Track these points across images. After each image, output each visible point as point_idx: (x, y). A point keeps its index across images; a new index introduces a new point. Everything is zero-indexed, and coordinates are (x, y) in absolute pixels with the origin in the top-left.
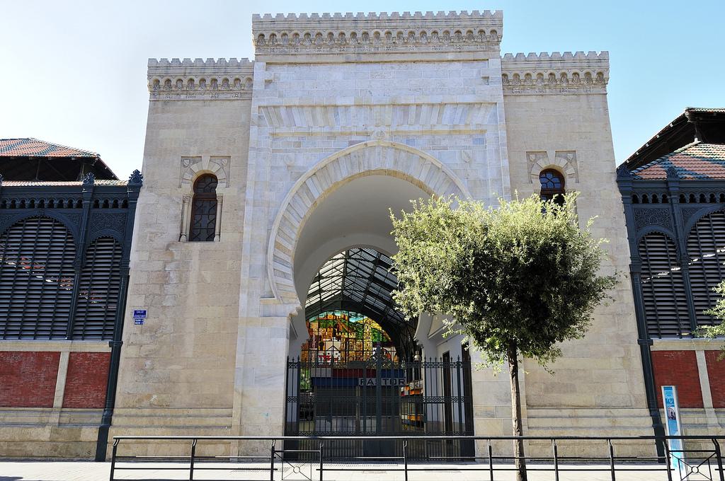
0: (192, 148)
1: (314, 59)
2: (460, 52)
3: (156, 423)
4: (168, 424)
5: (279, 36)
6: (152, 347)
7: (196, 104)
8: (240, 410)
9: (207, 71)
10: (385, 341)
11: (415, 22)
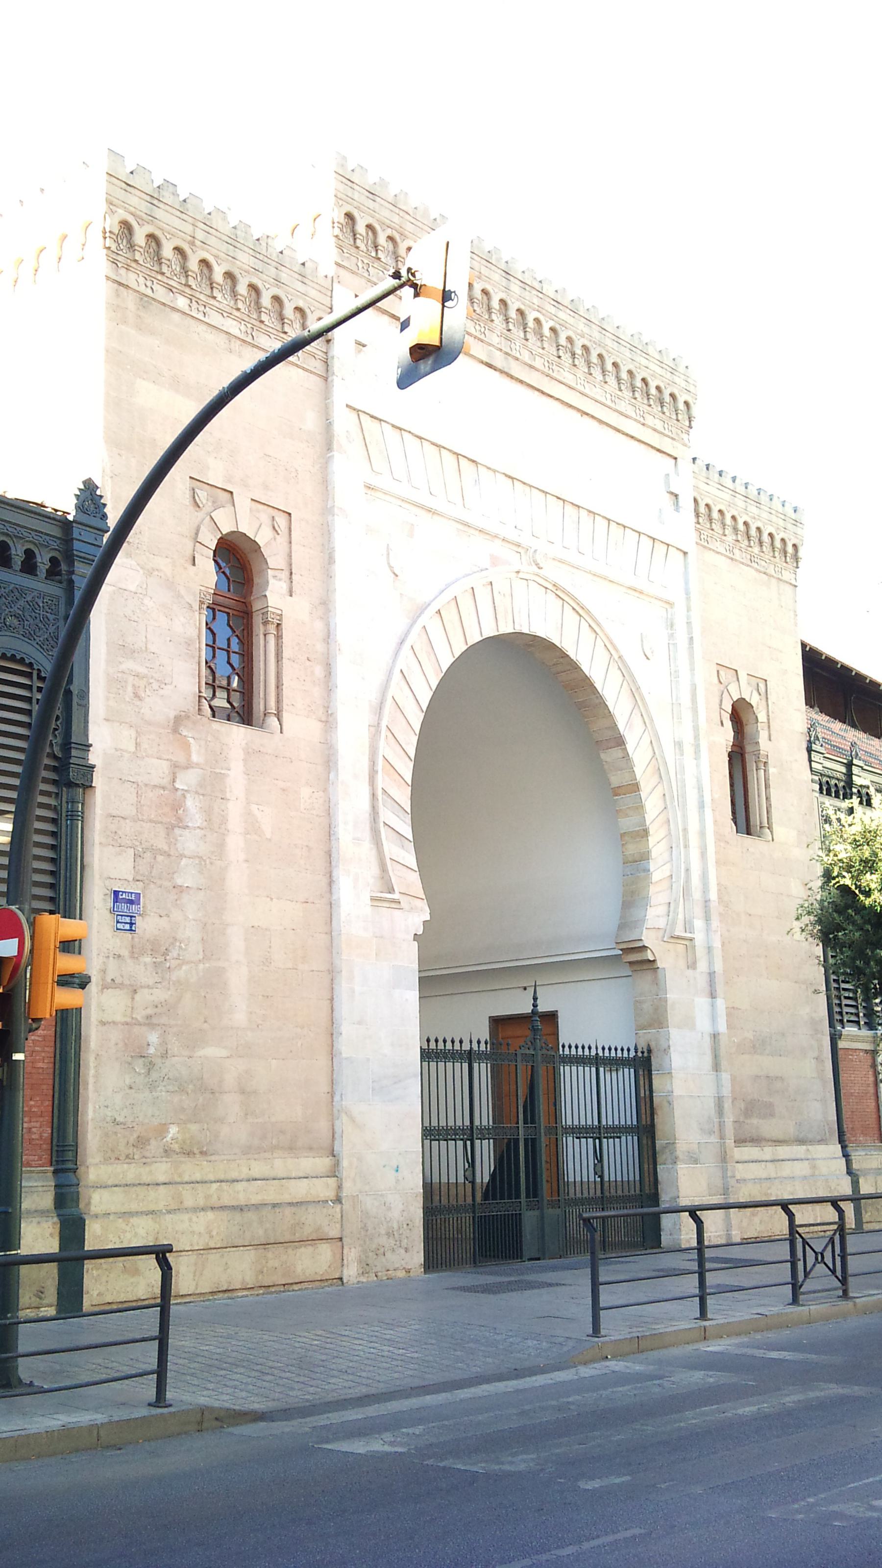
3: (189, 1202)
4: (214, 1201)
6: (160, 995)
7: (212, 337)
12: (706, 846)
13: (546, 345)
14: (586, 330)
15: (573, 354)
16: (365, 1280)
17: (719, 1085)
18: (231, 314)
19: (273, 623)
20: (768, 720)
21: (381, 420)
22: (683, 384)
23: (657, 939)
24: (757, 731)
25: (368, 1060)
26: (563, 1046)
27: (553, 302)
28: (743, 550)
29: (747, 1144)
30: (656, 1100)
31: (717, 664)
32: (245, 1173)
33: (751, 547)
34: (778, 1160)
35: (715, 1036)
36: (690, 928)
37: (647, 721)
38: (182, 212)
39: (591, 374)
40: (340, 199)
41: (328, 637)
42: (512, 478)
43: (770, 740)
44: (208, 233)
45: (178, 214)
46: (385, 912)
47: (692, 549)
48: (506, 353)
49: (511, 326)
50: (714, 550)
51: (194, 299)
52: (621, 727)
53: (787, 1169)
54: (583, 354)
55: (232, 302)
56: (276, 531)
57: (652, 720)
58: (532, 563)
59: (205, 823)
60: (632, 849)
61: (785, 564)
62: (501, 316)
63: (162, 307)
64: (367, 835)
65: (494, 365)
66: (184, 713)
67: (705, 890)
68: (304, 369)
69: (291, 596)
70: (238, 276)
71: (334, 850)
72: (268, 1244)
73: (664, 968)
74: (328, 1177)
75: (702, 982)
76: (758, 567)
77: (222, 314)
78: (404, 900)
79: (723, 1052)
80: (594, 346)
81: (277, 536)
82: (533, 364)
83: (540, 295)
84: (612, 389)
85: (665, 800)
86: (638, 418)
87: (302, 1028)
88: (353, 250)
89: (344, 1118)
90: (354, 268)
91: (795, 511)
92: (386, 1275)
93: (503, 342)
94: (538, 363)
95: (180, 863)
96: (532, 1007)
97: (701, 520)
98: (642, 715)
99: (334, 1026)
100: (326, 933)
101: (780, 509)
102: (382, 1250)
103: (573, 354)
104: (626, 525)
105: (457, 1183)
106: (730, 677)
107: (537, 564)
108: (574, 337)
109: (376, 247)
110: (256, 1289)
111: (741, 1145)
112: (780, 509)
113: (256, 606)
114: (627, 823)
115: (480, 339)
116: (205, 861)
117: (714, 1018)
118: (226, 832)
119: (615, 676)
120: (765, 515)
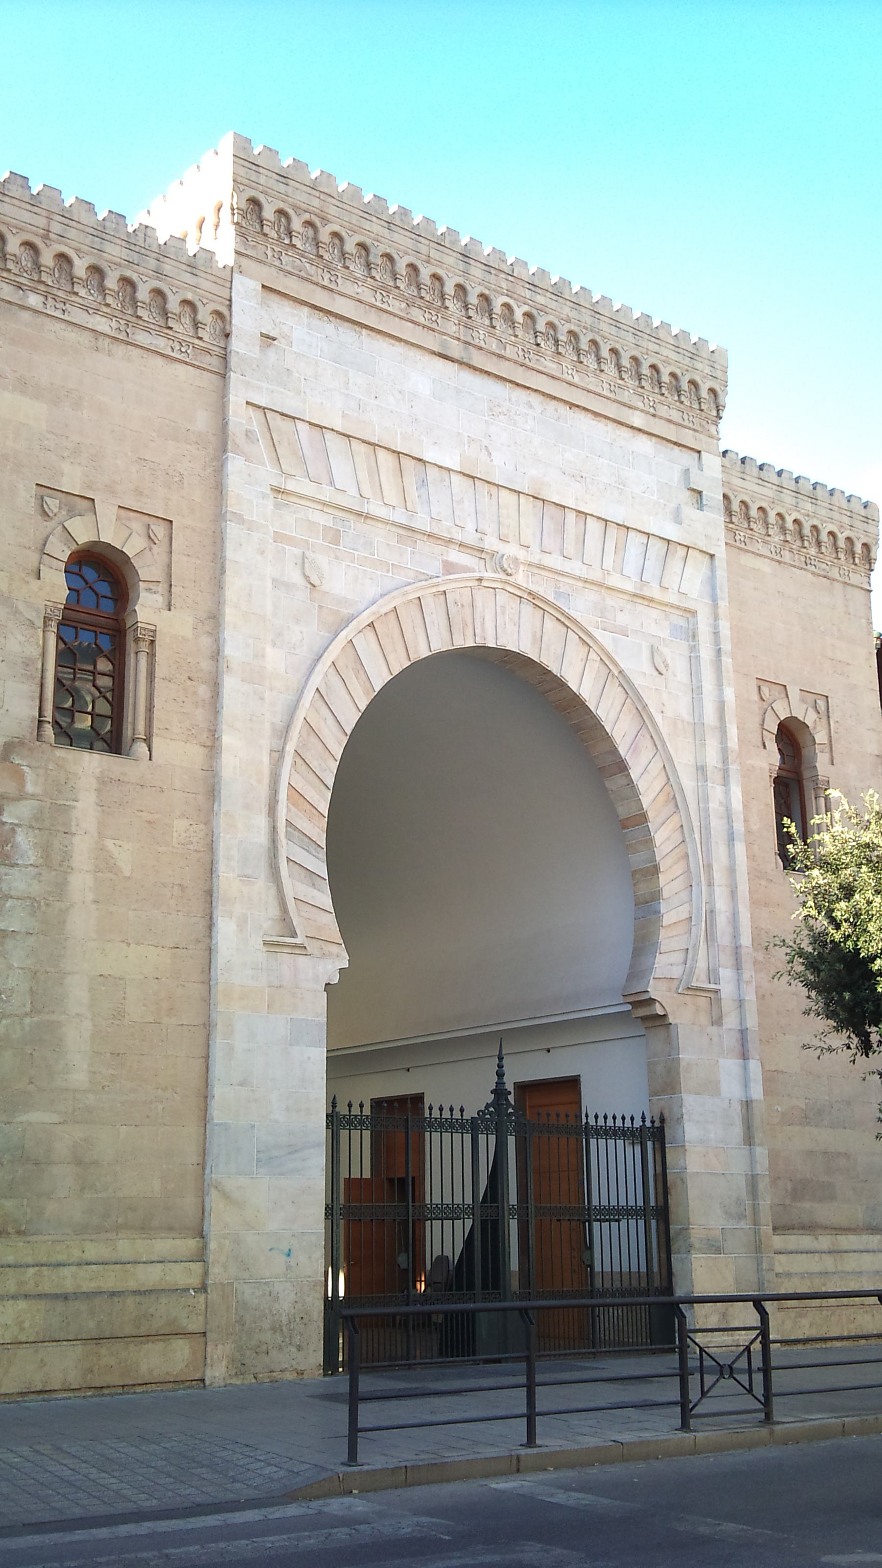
0: (66, 467)
1: (371, 319)
4: (30, 1288)
7: (72, 335)
9: (108, 247)
12: (736, 884)
13: (519, 332)
14: (573, 314)
15: (557, 341)
16: (239, 1382)
17: (752, 1161)
18: (98, 310)
19: (144, 640)
20: (830, 741)
21: (294, 418)
22: (707, 370)
23: (670, 990)
24: (815, 754)
25: (253, 1126)
26: (431, 1108)
27: (527, 286)
28: (795, 552)
29: (795, 1231)
30: (670, 1178)
31: (757, 678)
32: (76, 1254)
33: (805, 548)
34: (840, 1252)
35: (747, 1104)
36: (715, 978)
37: (658, 744)
38: (33, 205)
39: (581, 362)
40: (241, 184)
41: (216, 655)
42: (348, 436)
43: (833, 764)
44: (68, 226)
45: (28, 207)
46: (285, 959)
47: (721, 552)
48: (466, 343)
49: (471, 313)
50: (753, 553)
51: (50, 296)
52: (622, 751)
53: (851, 1263)
54: (571, 341)
55: (100, 298)
56: (153, 540)
58: (499, 569)
59: (41, 860)
60: (644, 889)
61: (853, 566)
62: (459, 303)
63: (7, 306)
64: (263, 871)
65: (449, 355)
66: (17, 740)
67: (736, 935)
68: (193, 366)
69: (170, 610)
70: (107, 269)
71: (215, 889)
72: (103, 1339)
73: (676, 1025)
74: (192, 1261)
75: (731, 1041)
76: (816, 571)
77: (87, 310)
78: (313, 947)
79: (757, 1122)
80: (584, 331)
81: (153, 546)
82: (502, 353)
83: (510, 278)
84: (610, 378)
85: (683, 833)
86: (647, 408)
87: (165, 1089)
88: (260, 238)
89: (213, 1192)
90: (263, 258)
91: (865, 507)
93: (461, 331)
94: (510, 352)
95: (4, 904)
96: (497, 1068)
97: (734, 519)
98: (652, 737)
99: (209, 1087)
101: (845, 505)
102: (264, 1348)
103: (557, 341)
106: (777, 693)
107: (505, 571)
108: (556, 322)
109: (290, 234)
110: (83, 1390)
111: (787, 1232)
112: (845, 505)
113: (806, 774)
114: (638, 859)
115: (430, 329)
116: (39, 902)
117: (746, 1084)
118: (69, 870)
119: (614, 694)
120: (823, 512)
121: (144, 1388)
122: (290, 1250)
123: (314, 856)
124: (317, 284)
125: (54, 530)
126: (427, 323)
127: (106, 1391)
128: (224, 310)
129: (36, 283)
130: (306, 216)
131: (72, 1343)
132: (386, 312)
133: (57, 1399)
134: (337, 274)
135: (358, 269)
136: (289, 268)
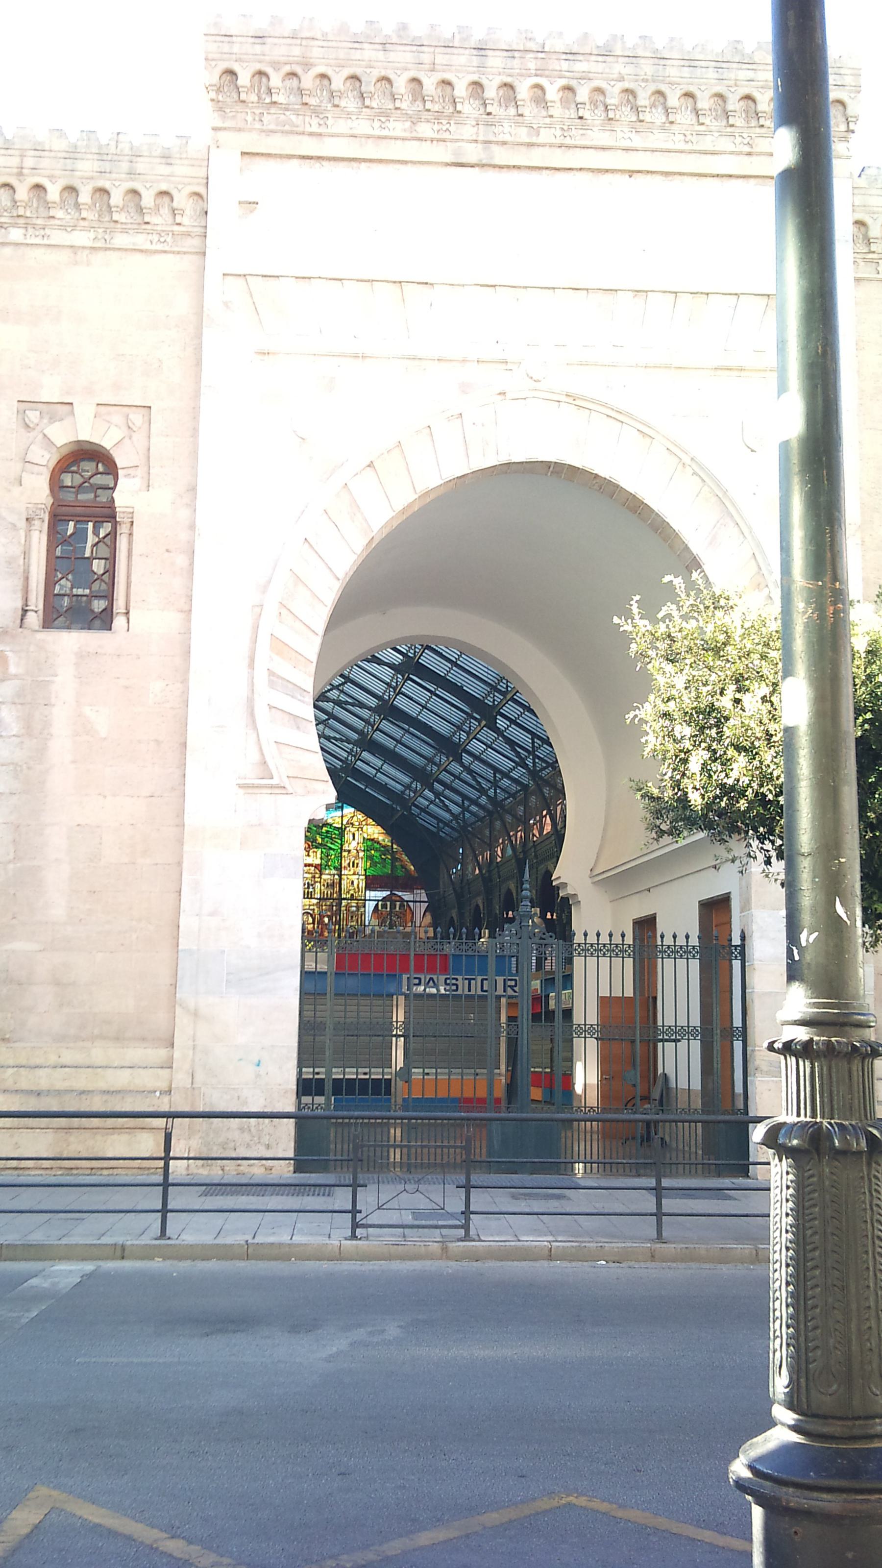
2: (749, 154)
5: (276, 80)
8: (191, 1052)
10: (400, 873)
11: (637, 65)
26: (662, 937)
27: (564, 56)
32: (53, 1059)
55: (77, 214)
57: (750, 528)
80: (643, 85)
81: (133, 433)
82: (534, 140)
83: (540, 55)
88: (239, 107)
92: (236, 1170)
94: (545, 136)
100: (177, 826)
102: (232, 1145)
104: (738, 292)
105: (689, 1089)
118: (49, 737)
121: (110, 1172)
122: (259, 1061)
123: (299, 700)
124: (303, 133)
125: (35, 438)
126: (435, 136)
127: (75, 1172)
128: (201, 190)
129: (16, 218)
130: (287, 69)
131: (45, 1130)
132: (385, 138)
133: (29, 1175)
134: (327, 115)
135: (350, 103)
136: (272, 127)
